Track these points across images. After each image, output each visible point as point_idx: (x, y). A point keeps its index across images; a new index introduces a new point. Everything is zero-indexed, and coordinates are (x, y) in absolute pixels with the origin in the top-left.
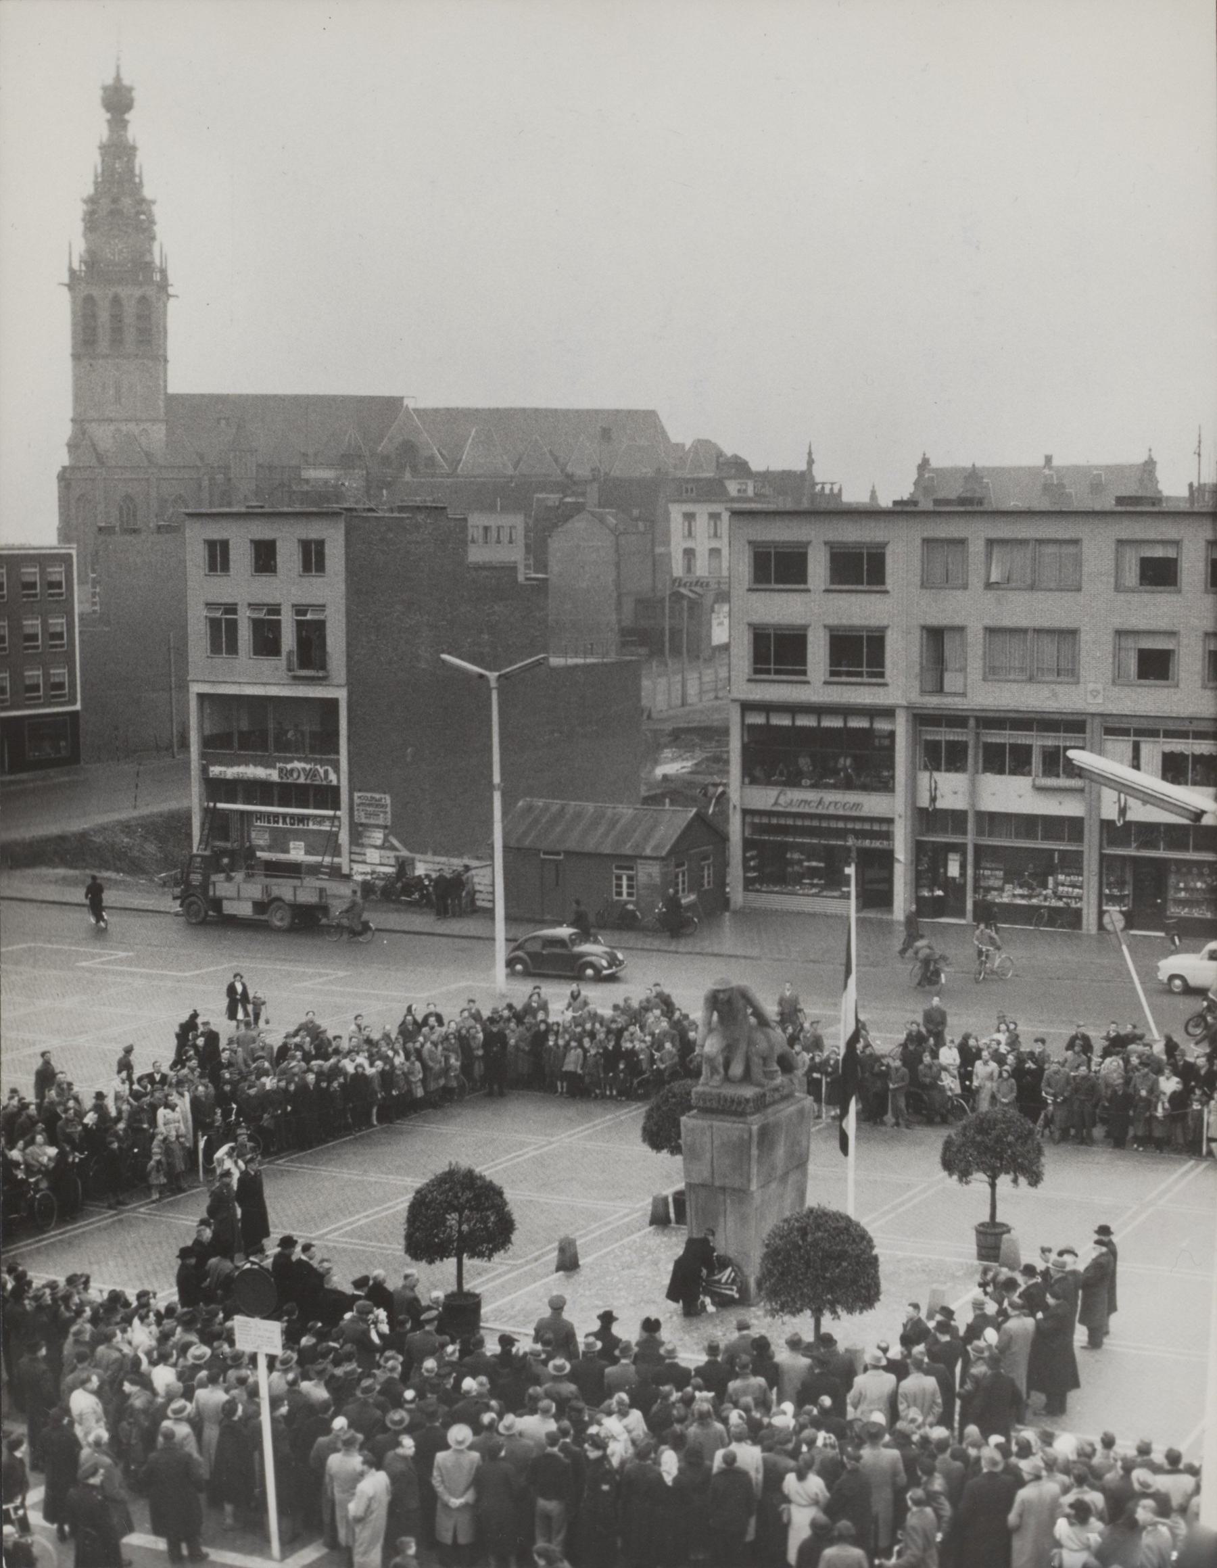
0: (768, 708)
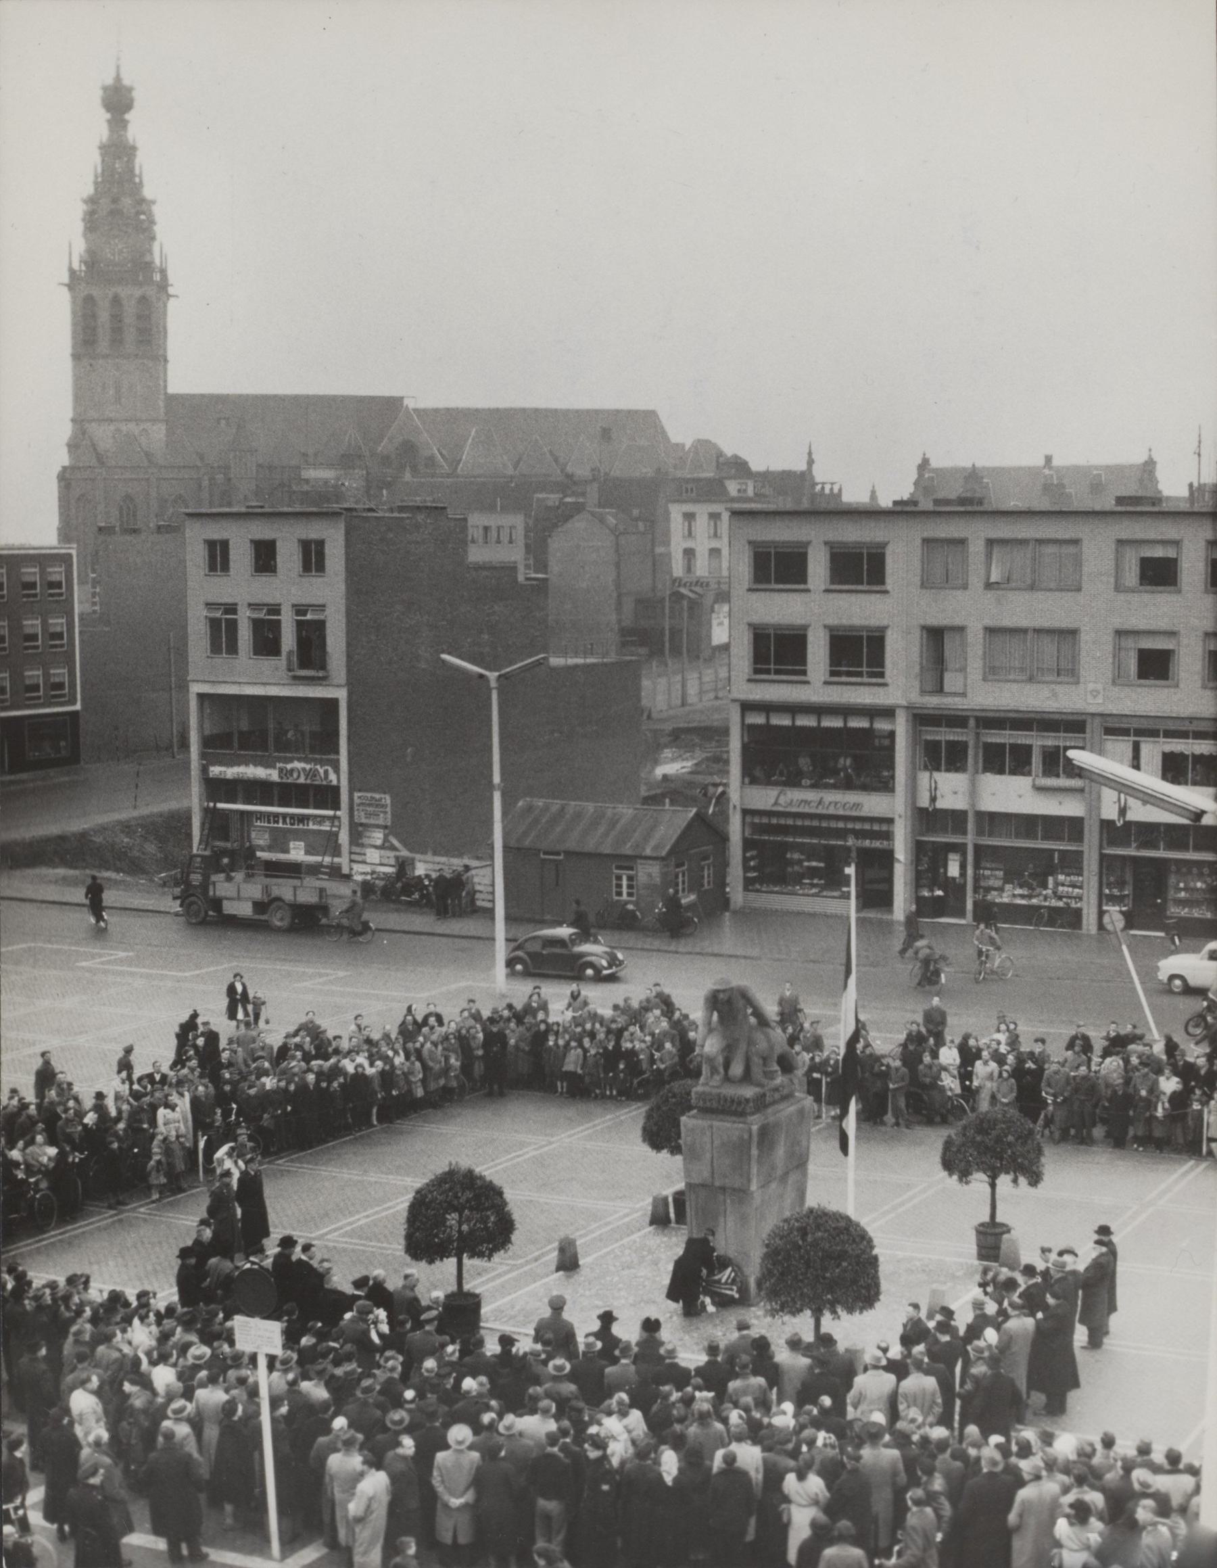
0: (768, 708)
